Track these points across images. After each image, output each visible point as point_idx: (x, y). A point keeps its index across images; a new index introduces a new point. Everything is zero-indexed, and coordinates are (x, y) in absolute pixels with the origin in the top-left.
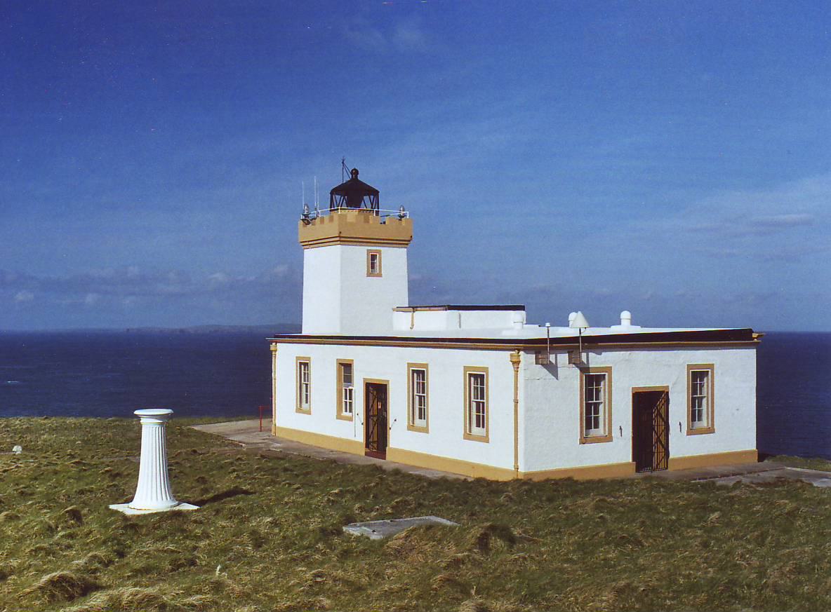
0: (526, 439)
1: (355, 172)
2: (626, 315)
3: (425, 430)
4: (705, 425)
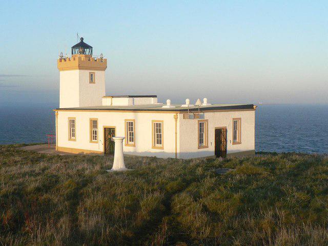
1: (82, 39)
2: (168, 101)
3: (75, 140)
4: (238, 141)
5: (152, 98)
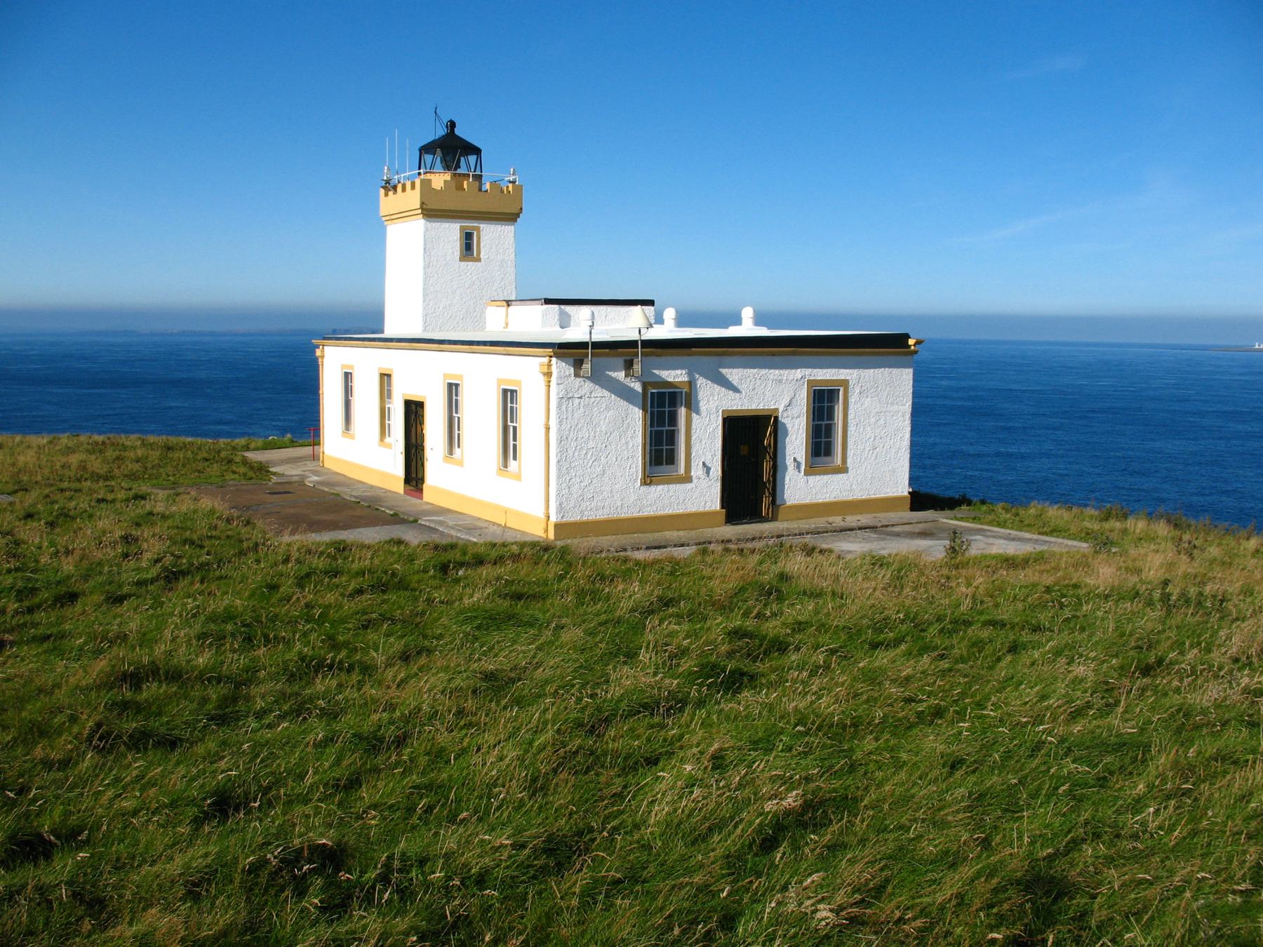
0: (559, 477)
1: (452, 125)
2: (747, 313)
5: (638, 309)
